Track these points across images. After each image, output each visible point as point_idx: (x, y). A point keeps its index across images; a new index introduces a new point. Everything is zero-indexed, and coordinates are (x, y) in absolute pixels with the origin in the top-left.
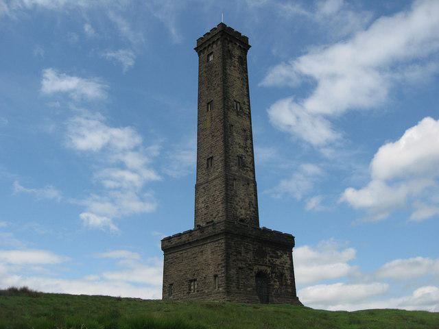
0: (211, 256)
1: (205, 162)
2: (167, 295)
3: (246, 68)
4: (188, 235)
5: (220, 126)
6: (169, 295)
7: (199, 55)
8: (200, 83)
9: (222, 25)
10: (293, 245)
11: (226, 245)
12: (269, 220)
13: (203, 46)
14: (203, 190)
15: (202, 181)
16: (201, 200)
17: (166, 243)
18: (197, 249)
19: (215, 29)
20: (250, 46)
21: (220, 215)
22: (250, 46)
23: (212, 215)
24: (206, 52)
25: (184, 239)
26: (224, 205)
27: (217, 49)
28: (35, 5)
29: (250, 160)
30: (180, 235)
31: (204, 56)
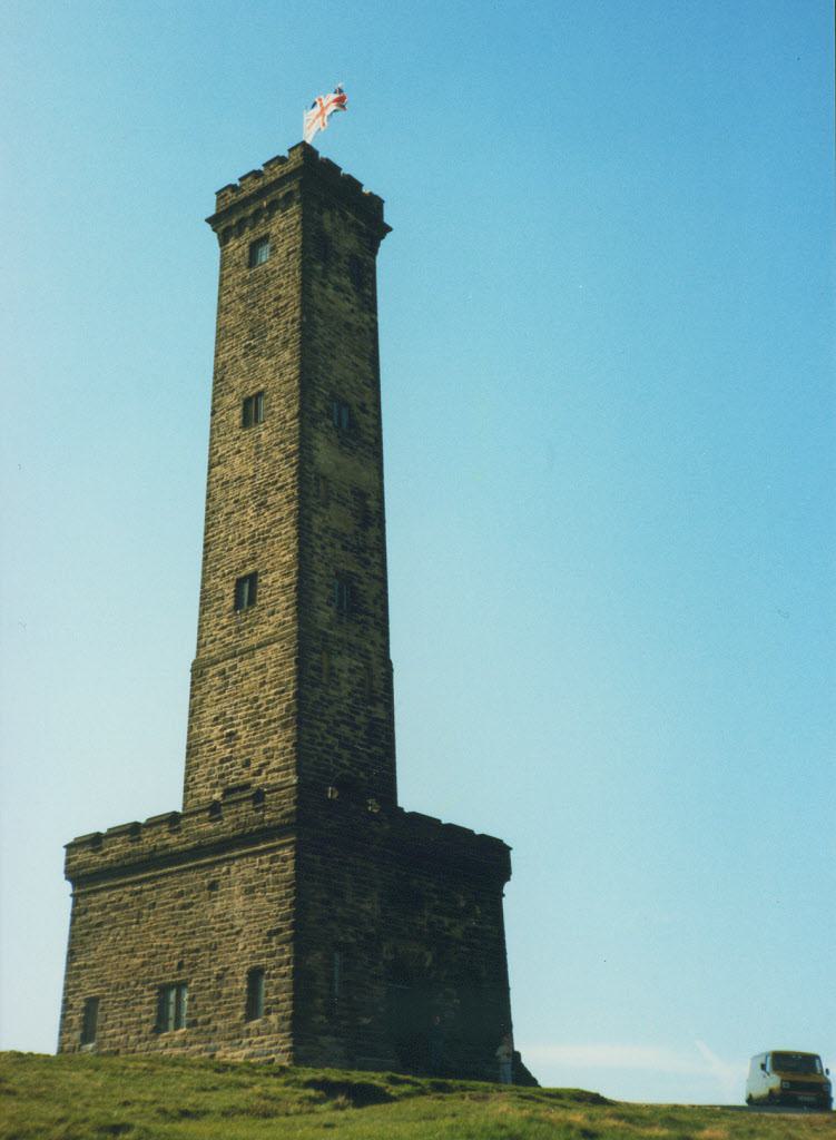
0: (248, 906)
1: (229, 590)
2: (77, 1035)
3: (373, 298)
4: (165, 828)
5: (287, 474)
6: (86, 1039)
7: (223, 241)
8: (222, 334)
9: (307, 150)
10: (505, 873)
11: (297, 866)
12: (430, 782)
13: (236, 214)
14: (217, 681)
15: (215, 650)
16: (210, 713)
17: (83, 856)
18: (199, 879)
19: (281, 160)
20: (389, 229)
21: (274, 764)
22: (389, 229)
23: (247, 764)
24: (249, 235)
25: (149, 841)
26: (290, 733)
27: (285, 227)
28: (504, 895)
29: (371, 347)
30: (134, 830)
31: (239, 246)
